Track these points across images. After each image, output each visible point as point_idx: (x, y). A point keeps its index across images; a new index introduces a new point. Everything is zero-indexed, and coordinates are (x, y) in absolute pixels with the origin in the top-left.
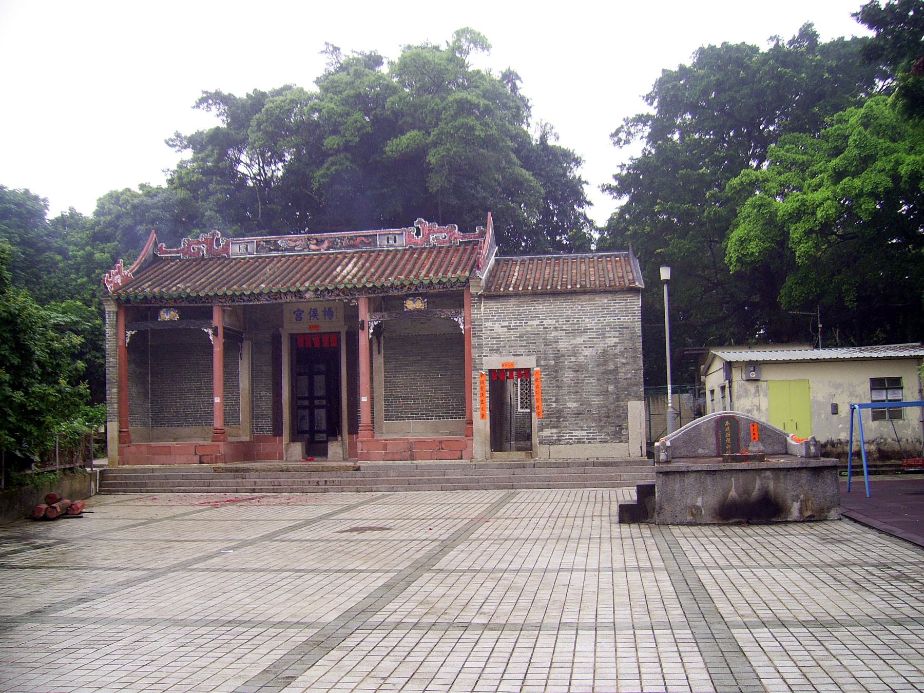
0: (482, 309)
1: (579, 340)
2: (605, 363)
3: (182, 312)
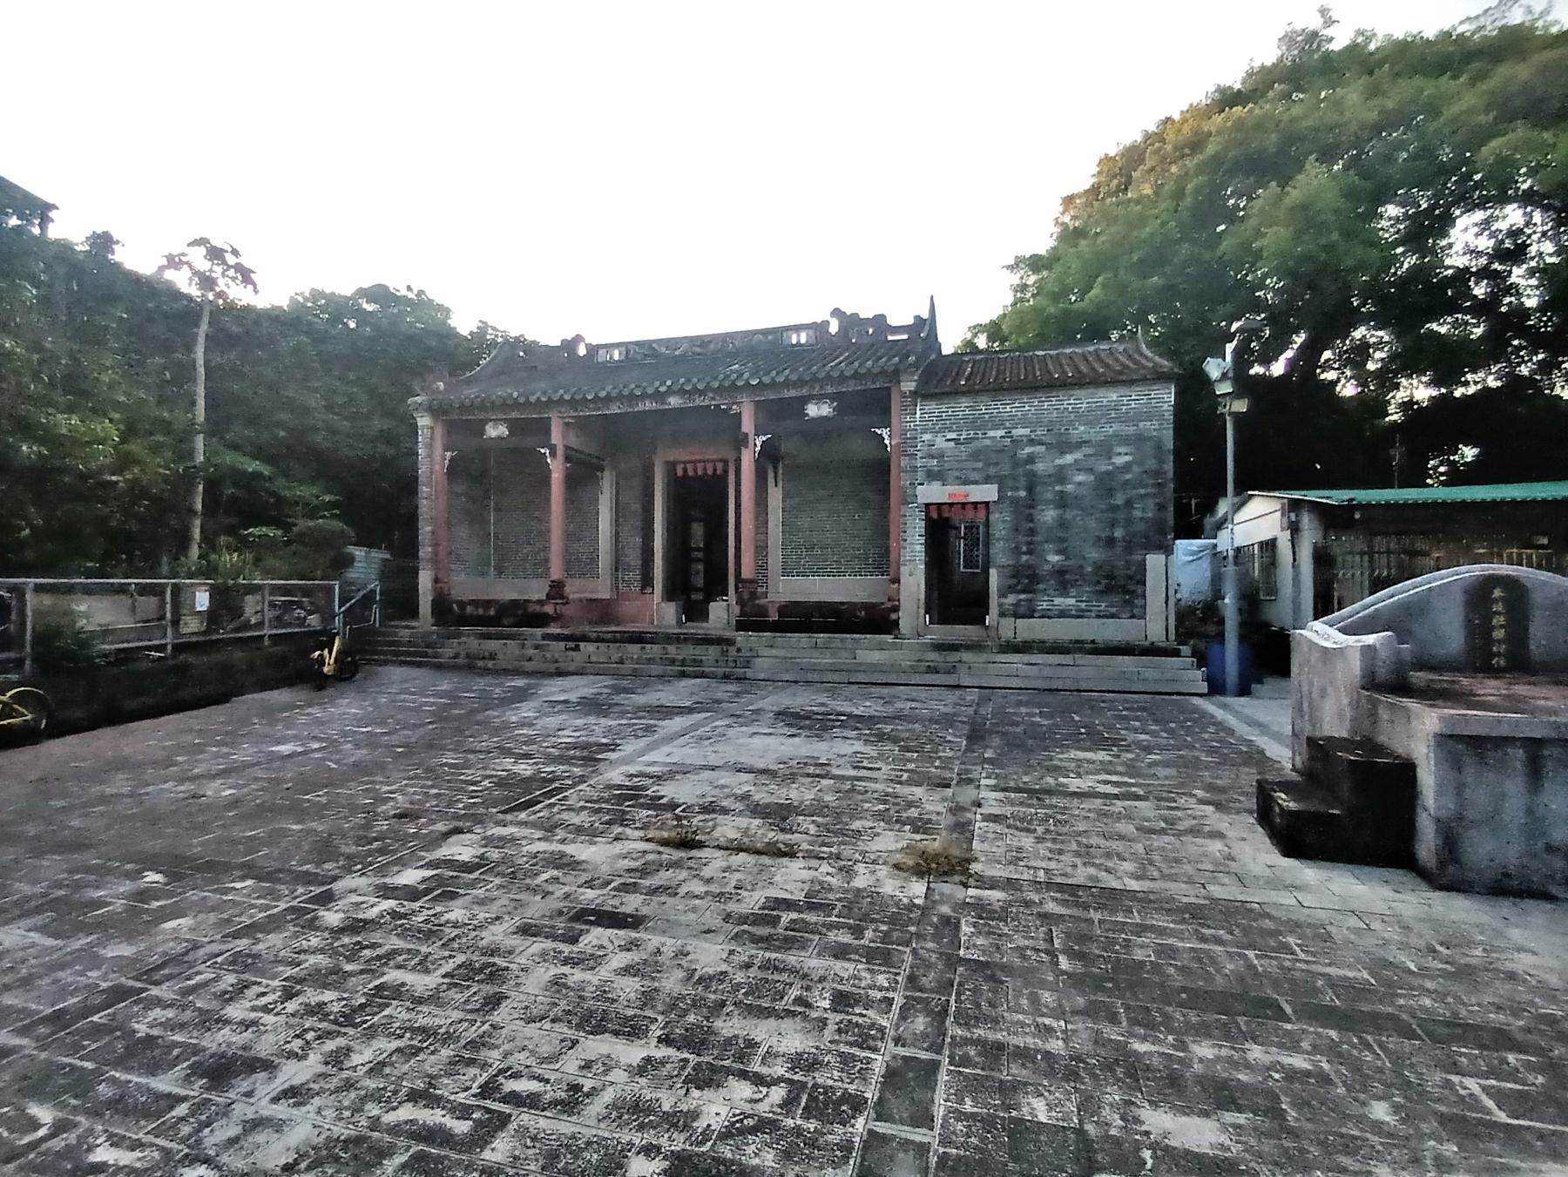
1: (1069, 459)
2: (1110, 492)
3: (513, 425)
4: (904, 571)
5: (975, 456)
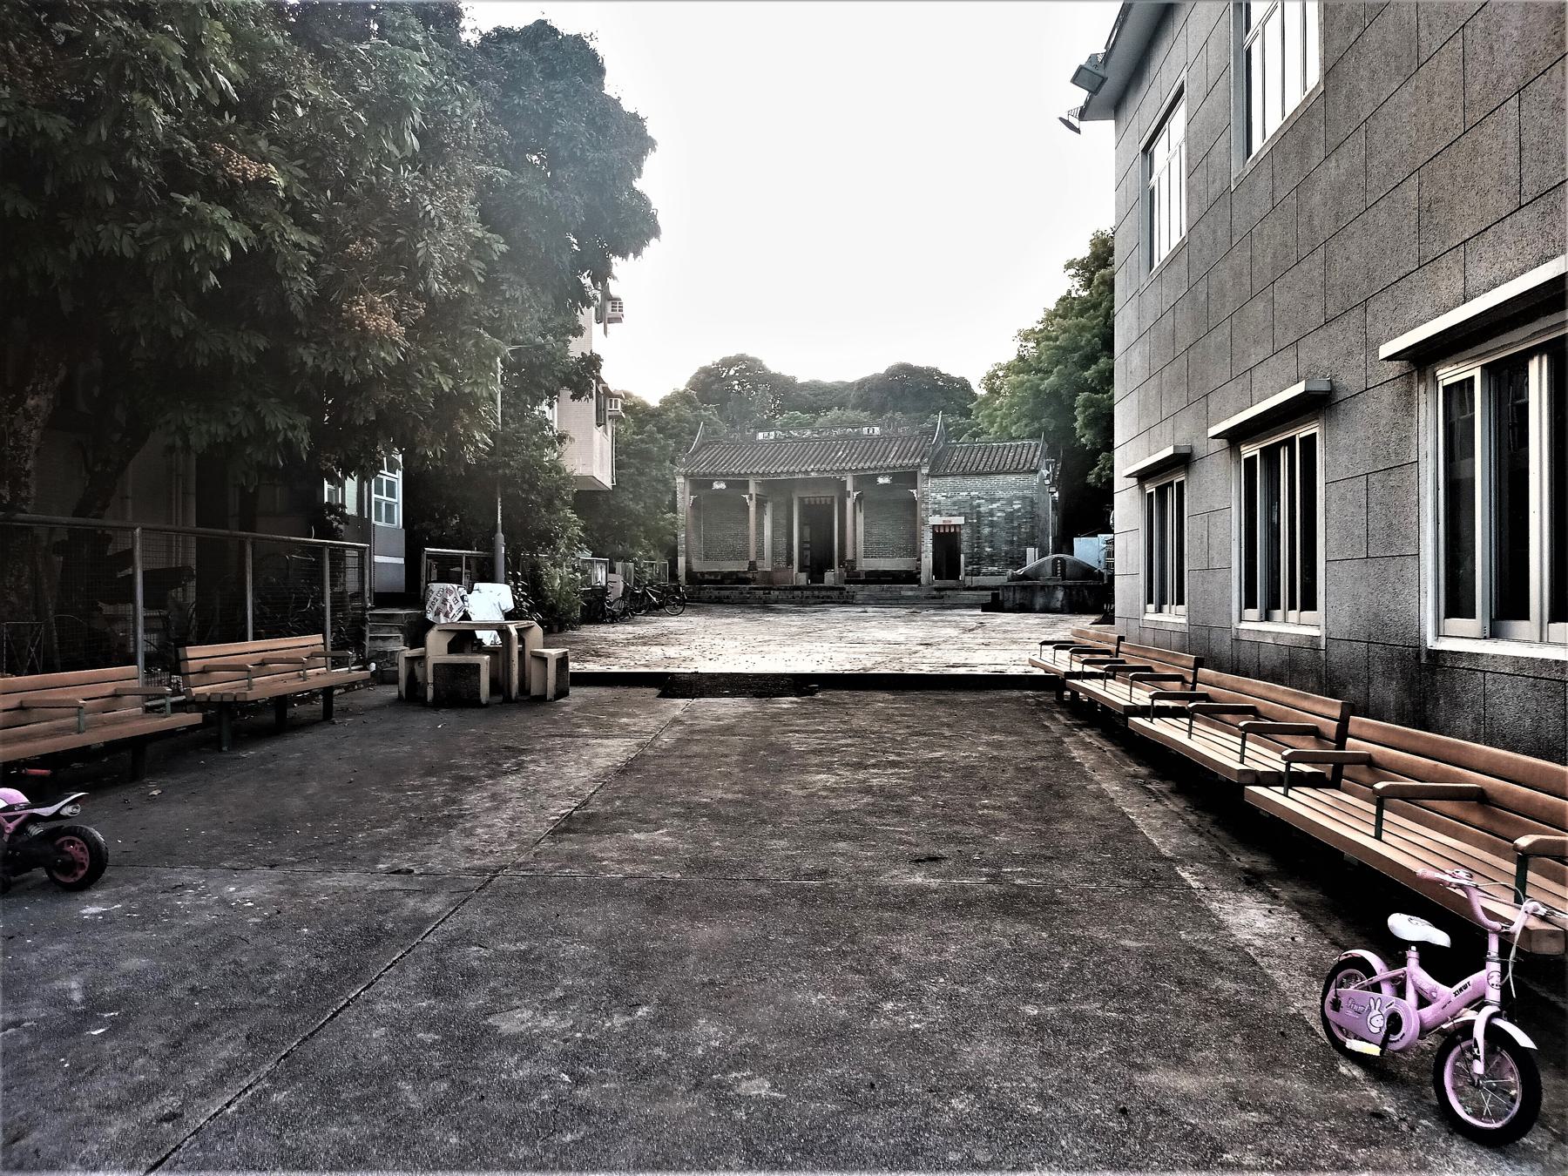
3: (728, 484)
5: (954, 504)
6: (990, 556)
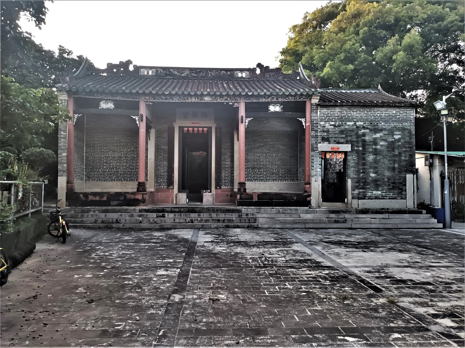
0: (319, 114)
1: (378, 135)
2: (393, 150)
4: (313, 179)
5: (342, 132)
6: (375, 181)
